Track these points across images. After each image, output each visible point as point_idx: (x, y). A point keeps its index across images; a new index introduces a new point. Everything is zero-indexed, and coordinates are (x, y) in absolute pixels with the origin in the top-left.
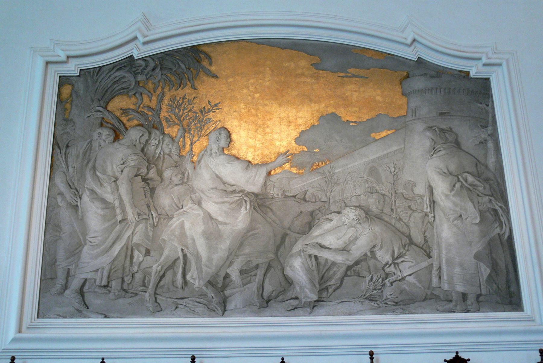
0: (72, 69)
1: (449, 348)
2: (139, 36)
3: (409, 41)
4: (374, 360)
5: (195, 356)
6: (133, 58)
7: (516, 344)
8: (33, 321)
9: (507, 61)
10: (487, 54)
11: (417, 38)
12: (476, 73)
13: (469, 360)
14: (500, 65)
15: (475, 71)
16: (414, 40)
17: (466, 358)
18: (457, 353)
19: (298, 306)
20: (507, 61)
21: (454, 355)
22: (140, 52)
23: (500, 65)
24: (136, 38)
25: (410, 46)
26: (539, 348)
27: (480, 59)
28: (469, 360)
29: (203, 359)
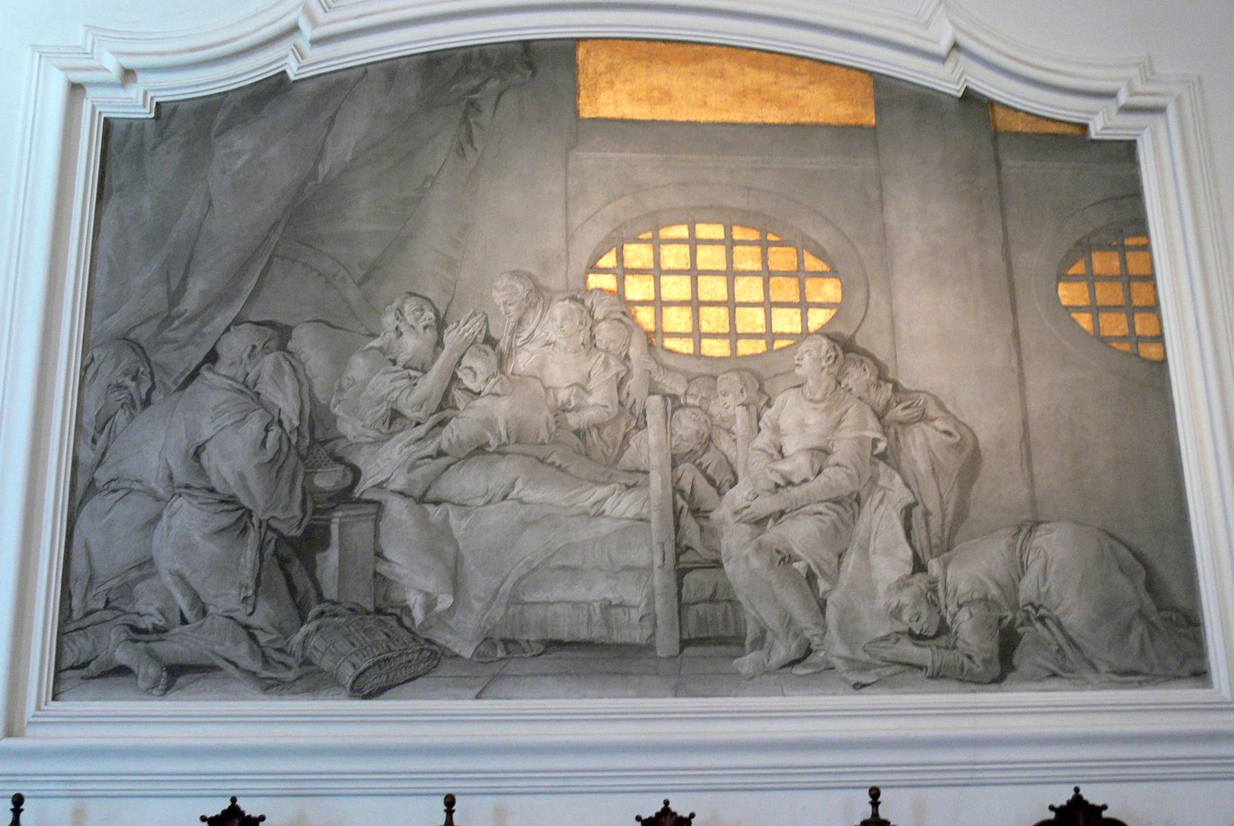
0: (133, 104)
1: (671, 781)
2: (304, 25)
3: (943, 47)
4: (22, 815)
5: (24, 793)
6: (288, 78)
7: (892, 772)
8: (43, 707)
9: (1178, 100)
10: (1130, 83)
11: (964, 41)
12: (1104, 128)
13: (262, 818)
14: (1159, 110)
15: (1103, 124)
16: (956, 46)
17: (256, 814)
18: (234, 800)
19: (966, 678)
20: (1178, 100)
21: (226, 804)
22: (303, 62)
23: (1159, 110)
24: (295, 29)
25: (942, 59)
26: (872, 784)
27: (1112, 95)
28: (262, 818)
29: (85, 800)
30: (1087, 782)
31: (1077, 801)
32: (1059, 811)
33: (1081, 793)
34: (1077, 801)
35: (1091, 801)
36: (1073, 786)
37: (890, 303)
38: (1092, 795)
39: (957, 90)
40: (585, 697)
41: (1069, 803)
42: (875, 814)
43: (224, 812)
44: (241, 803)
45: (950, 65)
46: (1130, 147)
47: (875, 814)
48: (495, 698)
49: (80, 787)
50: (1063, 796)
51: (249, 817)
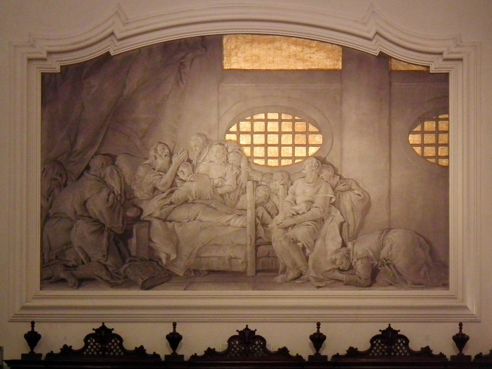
5: (34, 321)
16: (377, 33)
27: (441, 54)
31: (103, 327)
34: (103, 327)
35: (108, 328)
39: (376, 53)
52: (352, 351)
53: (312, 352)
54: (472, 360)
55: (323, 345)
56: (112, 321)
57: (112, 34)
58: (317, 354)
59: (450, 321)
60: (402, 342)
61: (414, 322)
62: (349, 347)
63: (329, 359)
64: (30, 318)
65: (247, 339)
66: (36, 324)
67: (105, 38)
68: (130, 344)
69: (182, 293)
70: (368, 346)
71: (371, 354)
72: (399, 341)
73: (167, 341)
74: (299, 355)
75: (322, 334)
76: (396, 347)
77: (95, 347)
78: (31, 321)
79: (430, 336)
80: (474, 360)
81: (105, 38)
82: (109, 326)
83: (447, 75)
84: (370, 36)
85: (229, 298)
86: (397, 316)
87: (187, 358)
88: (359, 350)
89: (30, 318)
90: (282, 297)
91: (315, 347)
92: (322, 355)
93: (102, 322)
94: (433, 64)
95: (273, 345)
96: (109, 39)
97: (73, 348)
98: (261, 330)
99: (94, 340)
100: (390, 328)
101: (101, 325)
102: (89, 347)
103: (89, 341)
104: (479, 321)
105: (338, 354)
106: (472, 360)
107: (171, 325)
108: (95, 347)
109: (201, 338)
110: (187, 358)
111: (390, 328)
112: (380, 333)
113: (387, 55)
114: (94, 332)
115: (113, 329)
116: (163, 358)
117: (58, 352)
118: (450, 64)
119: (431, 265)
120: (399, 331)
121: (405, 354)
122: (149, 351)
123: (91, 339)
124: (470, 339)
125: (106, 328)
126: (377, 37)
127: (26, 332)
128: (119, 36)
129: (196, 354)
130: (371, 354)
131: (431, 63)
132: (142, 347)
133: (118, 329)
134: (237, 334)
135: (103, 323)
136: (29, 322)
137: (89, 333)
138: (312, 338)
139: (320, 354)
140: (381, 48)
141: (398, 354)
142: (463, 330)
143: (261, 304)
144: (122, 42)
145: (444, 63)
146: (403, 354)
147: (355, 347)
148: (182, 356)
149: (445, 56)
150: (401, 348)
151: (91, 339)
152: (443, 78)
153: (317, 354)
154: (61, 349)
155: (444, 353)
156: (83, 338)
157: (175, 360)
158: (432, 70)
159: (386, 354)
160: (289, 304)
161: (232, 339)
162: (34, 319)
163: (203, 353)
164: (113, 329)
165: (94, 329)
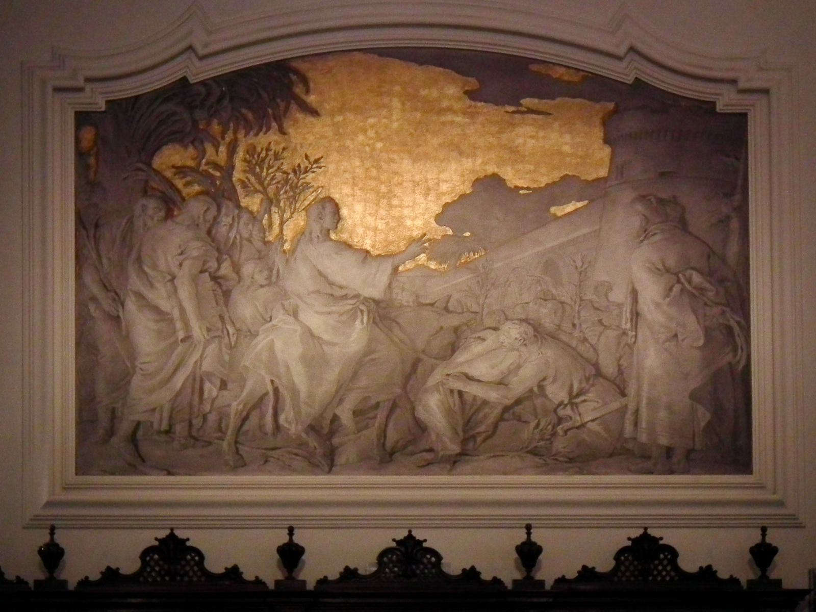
3: (622, 51)
4: (532, 535)
5: (294, 526)
15: (726, 101)
16: (632, 49)
25: (619, 58)
27: (734, 82)
30: (417, 528)
31: (172, 536)
32: (399, 542)
33: (412, 533)
34: (172, 536)
35: (417, 538)
36: (408, 530)
37: (240, 254)
38: (418, 535)
39: (630, 80)
40: (281, 475)
41: (405, 538)
42: (291, 539)
43: (405, 537)
44: (414, 533)
45: (624, 64)
46: (743, 117)
47: (291, 539)
48: (459, 474)
49: (700, 522)
50: (401, 534)
51: (418, 540)
52: (111, 574)
53: (41, 575)
54: (33, 589)
55: (61, 563)
56: (564, 526)
57: (190, 48)
58: (51, 579)
59: (360, 526)
60: (666, 557)
61: (153, 528)
62: (344, 567)
63: (548, 586)
64: (286, 523)
65: (410, 553)
66: (296, 531)
67: (173, 58)
68: (216, 565)
69: (445, 479)
70: (138, 565)
71: (616, 579)
72: (662, 556)
73: (39, 557)
74: (734, 576)
75: (535, 544)
76: (656, 567)
77: (632, 568)
78: (288, 526)
79: (708, 547)
80: (552, 587)
81: (173, 58)
82: (181, 534)
83: (744, 116)
84: (622, 51)
85: (358, 487)
86: (354, 518)
87: (72, 585)
88: (597, 570)
89: (286, 523)
90: (222, 487)
91: (758, 565)
92: (59, 579)
93: (408, 528)
94: (720, 97)
95: (454, 564)
96: (184, 56)
97: (121, 571)
98: (432, 539)
99: (630, 558)
100: (410, 537)
101: (168, 532)
102: (623, 568)
103: (148, 558)
104: (803, 525)
105: (564, 576)
106: (33, 589)
107: (759, 532)
108: (632, 568)
109: (330, 554)
110: (72, 585)
111: (410, 537)
112: (157, 543)
113: (170, 84)
114: (157, 543)
115: (188, 539)
116: (509, 585)
117: (575, 577)
118: (747, 97)
119: (721, 435)
120: (425, 541)
121: (672, 578)
122: (723, 574)
123: (626, 555)
124: (65, 551)
125: (177, 537)
126: (632, 55)
127: (519, 542)
128: (202, 51)
129: (87, 578)
130: (141, 579)
131: (717, 97)
132: (584, 567)
133: (195, 539)
134: (394, 545)
135: (172, 529)
136: (758, 527)
137: (199, 548)
138: (282, 550)
139: (532, 578)
140: (638, 72)
141: (659, 578)
142: (55, 537)
143: (524, 497)
144: (205, 62)
145: (740, 96)
146: (668, 578)
147: (241, 570)
148: (304, 582)
149: (742, 84)
150: (664, 569)
151: (667, 554)
152: (738, 124)
153: (51, 579)
154: (102, 573)
155: (262, 577)
156: (139, 554)
157: (529, 585)
158: (719, 108)
159: (167, 578)
160: (248, 499)
161: (146, 553)
162: (292, 522)
163: (338, 576)
164: (188, 539)
165: (629, 539)
